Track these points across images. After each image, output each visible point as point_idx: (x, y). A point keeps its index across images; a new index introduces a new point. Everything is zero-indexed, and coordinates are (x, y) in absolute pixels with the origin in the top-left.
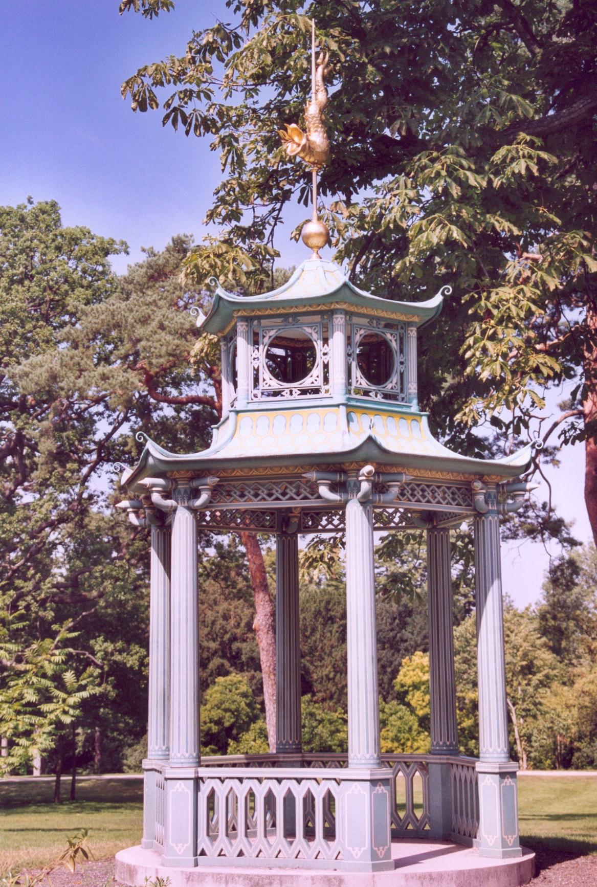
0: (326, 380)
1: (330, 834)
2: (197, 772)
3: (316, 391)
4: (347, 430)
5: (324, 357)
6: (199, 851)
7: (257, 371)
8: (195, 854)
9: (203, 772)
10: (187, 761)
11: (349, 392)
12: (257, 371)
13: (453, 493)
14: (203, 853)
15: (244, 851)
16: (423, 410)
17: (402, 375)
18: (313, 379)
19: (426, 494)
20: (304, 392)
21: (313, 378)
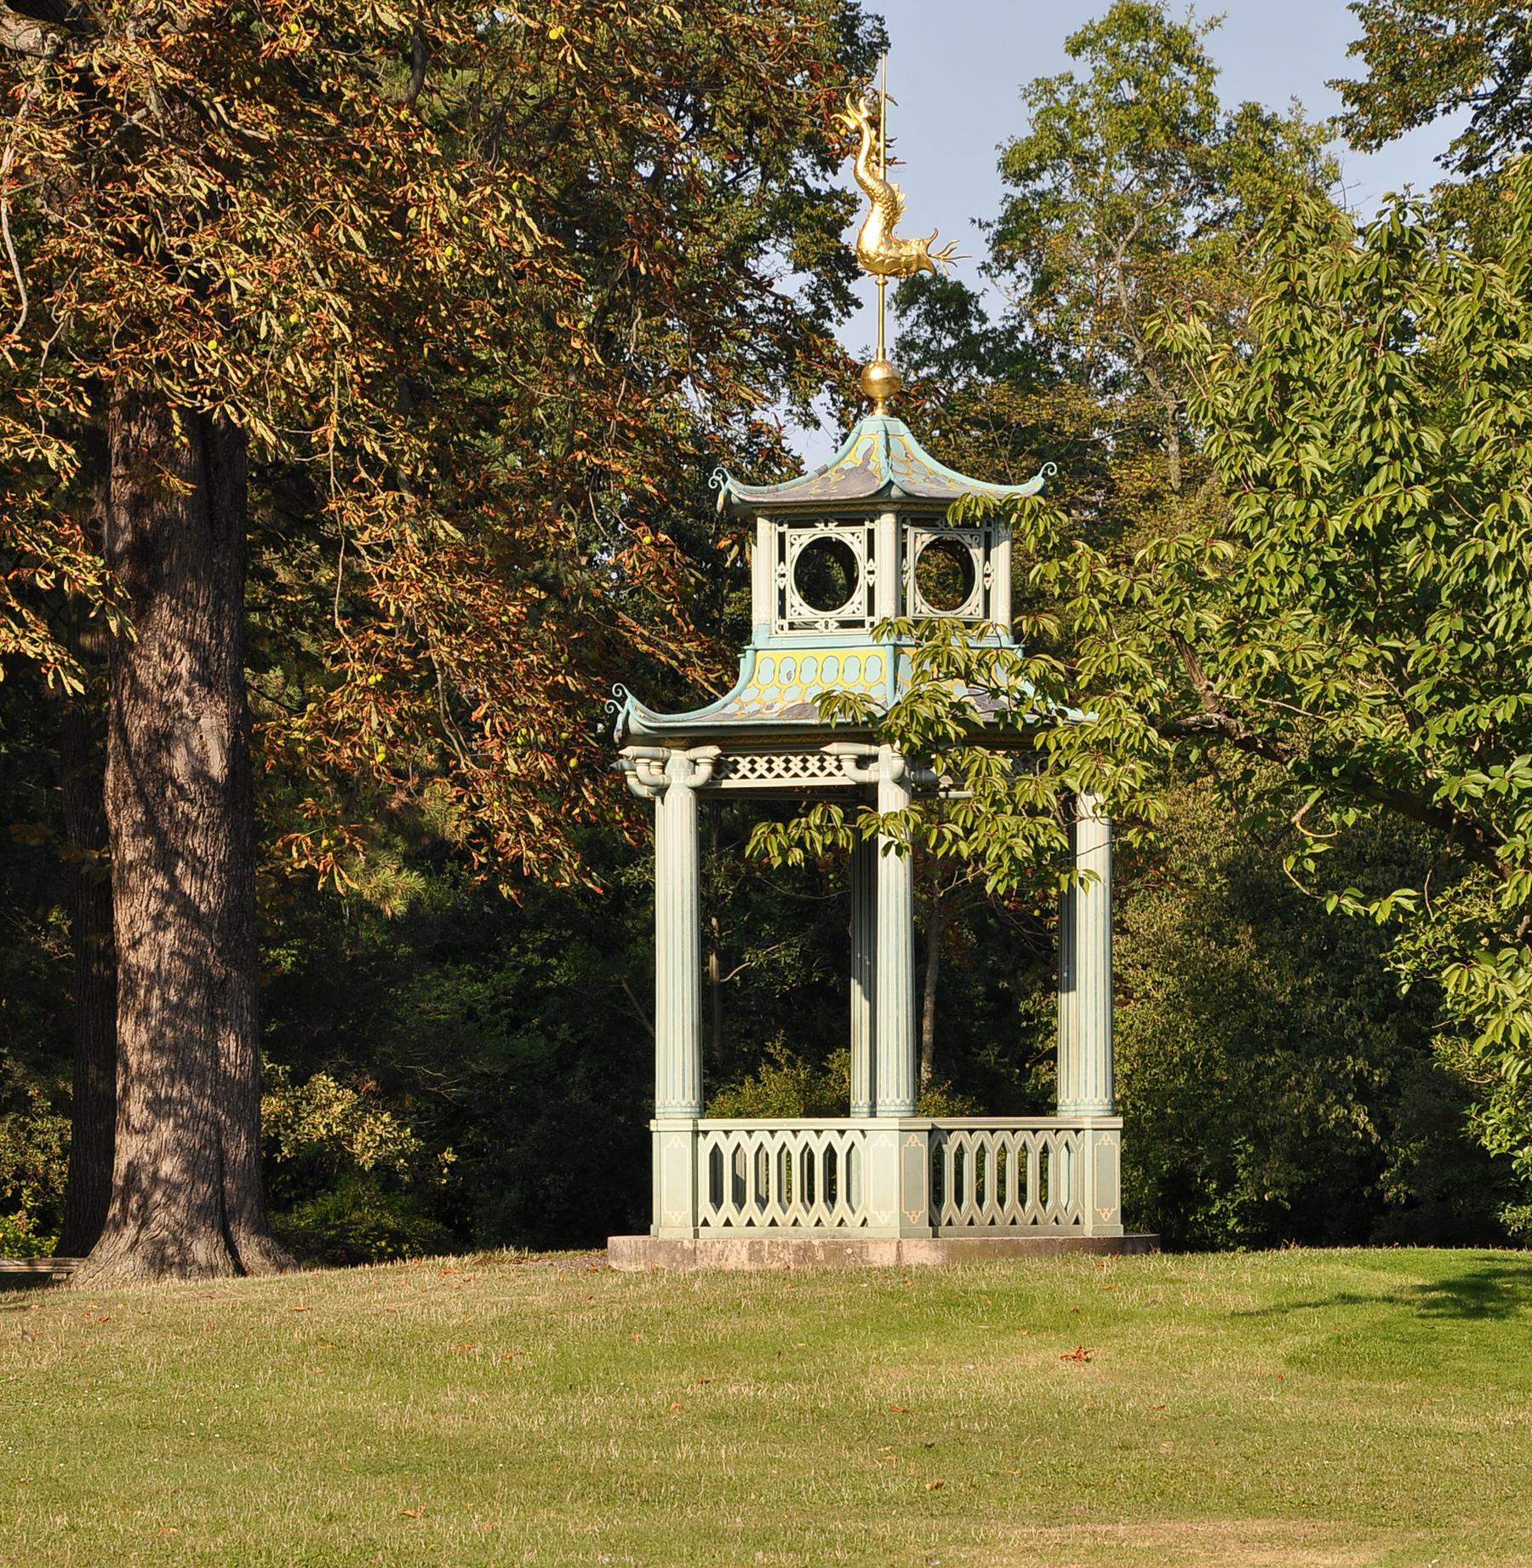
8: (695, 1224)
9: (704, 1124)
14: (706, 1223)
17: (987, 593)
18: (853, 608)
20: (845, 624)
21: (854, 607)
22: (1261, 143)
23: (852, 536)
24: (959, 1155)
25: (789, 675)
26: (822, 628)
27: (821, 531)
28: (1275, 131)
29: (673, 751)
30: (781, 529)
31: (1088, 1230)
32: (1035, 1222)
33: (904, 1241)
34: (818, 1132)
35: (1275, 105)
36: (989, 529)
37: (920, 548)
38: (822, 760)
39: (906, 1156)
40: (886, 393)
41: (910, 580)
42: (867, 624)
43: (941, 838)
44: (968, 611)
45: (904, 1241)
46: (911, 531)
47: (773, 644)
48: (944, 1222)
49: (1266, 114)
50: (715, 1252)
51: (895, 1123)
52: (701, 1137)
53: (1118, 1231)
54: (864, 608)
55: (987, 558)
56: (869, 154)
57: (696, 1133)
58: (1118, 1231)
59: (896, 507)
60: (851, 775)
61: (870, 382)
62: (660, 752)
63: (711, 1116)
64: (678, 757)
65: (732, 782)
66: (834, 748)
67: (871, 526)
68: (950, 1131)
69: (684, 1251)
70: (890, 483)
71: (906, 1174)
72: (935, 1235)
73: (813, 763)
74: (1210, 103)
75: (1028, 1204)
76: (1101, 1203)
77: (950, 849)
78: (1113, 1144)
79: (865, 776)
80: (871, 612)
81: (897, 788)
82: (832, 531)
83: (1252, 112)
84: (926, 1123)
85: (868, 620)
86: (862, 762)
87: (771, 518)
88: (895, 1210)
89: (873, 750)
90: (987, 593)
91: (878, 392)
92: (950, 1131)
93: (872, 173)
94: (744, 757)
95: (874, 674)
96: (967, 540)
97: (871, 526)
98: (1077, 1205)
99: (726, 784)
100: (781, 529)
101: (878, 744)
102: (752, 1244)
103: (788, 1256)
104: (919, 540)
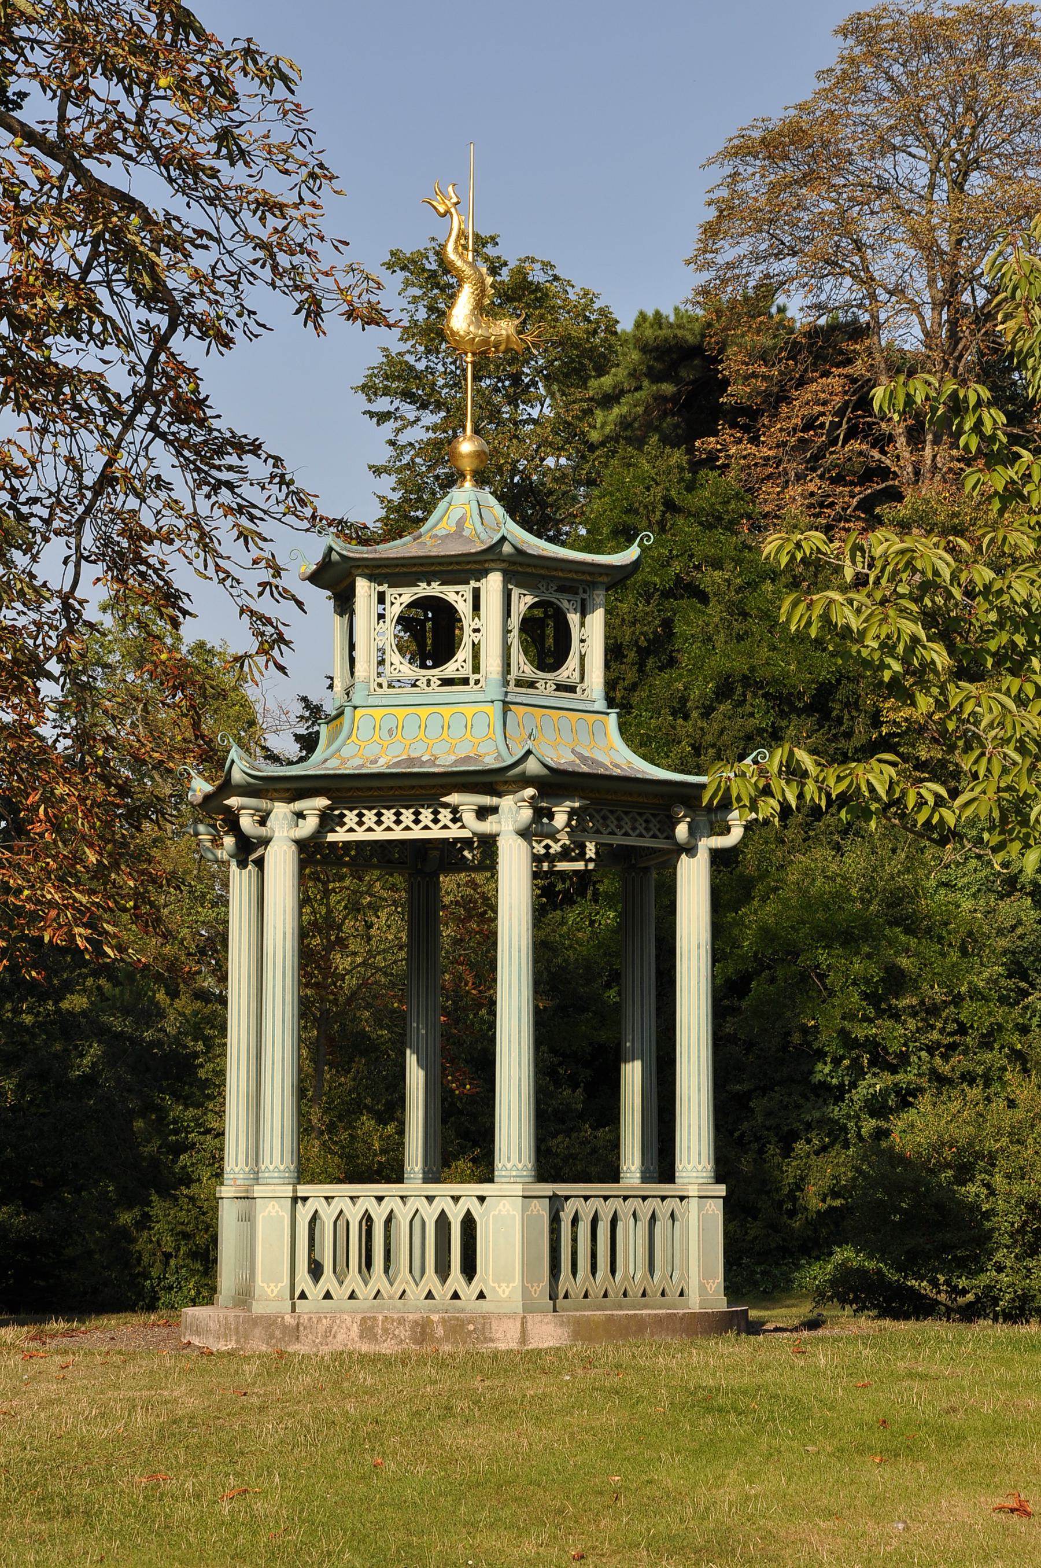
0: (476, 669)
1: (469, 1269)
2: (295, 1191)
3: (465, 681)
4: (578, 749)
5: (473, 635)
6: (297, 1294)
7: (382, 651)
8: (292, 1298)
9: (303, 1190)
10: (282, 1175)
11: (506, 683)
12: (382, 651)
13: (647, 821)
14: (303, 1296)
15: (357, 1291)
16: (610, 706)
17: (582, 658)
18: (458, 665)
19: (651, 826)
20: (447, 682)
21: (458, 665)
22: (206, 661)
23: (457, 596)
24: (575, 1221)
25: (390, 731)
26: (424, 686)
27: (424, 590)
28: (214, 655)
29: (276, 804)
30: (381, 589)
31: (694, 1304)
32: (644, 1295)
33: (529, 1316)
34: (380, 1199)
35: (213, 642)
36: (585, 596)
37: (523, 609)
38: (436, 813)
39: (528, 1223)
40: (474, 467)
41: (514, 638)
42: (472, 682)
43: (921, 803)
44: (565, 674)
45: (529, 1316)
46: (515, 592)
47: (371, 701)
48: (561, 1295)
49: (208, 646)
50: (321, 1329)
51: (518, 1189)
52: (299, 1204)
53: (720, 1303)
54: (469, 666)
55: (582, 624)
56: (458, 237)
57: (295, 1199)
58: (720, 1303)
59: (504, 565)
60: (473, 825)
61: (460, 455)
62: (263, 804)
63: (311, 1182)
64: (281, 811)
65: (339, 836)
66: (453, 799)
67: (477, 585)
68: (567, 1198)
69: (284, 1327)
70: (503, 539)
71: (528, 1243)
72: (555, 1311)
73: (426, 815)
74: (179, 639)
75: (600, 1274)
76: (706, 1274)
77: (931, 816)
78: (716, 1209)
79: (487, 827)
80: (476, 669)
81: (520, 841)
82: (435, 589)
83: (201, 645)
84: (547, 1189)
85: (473, 678)
86: (483, 813)
87: (371, 578)
88: (517, 1282)
89: (493, 801)
90: (582, 658)
91: (467, 466)
92: (567, 1198)
93: (461, 256)
94: (351, 810)
95: (481, 730)
96: (565, 605)
97: (477, 585)
98: (682, 1277)
99: (331, 837)
100: (381, 589)
101: (500, 795)
102: (364, 1320)
103: (403, 1333)
104: (523, 602)
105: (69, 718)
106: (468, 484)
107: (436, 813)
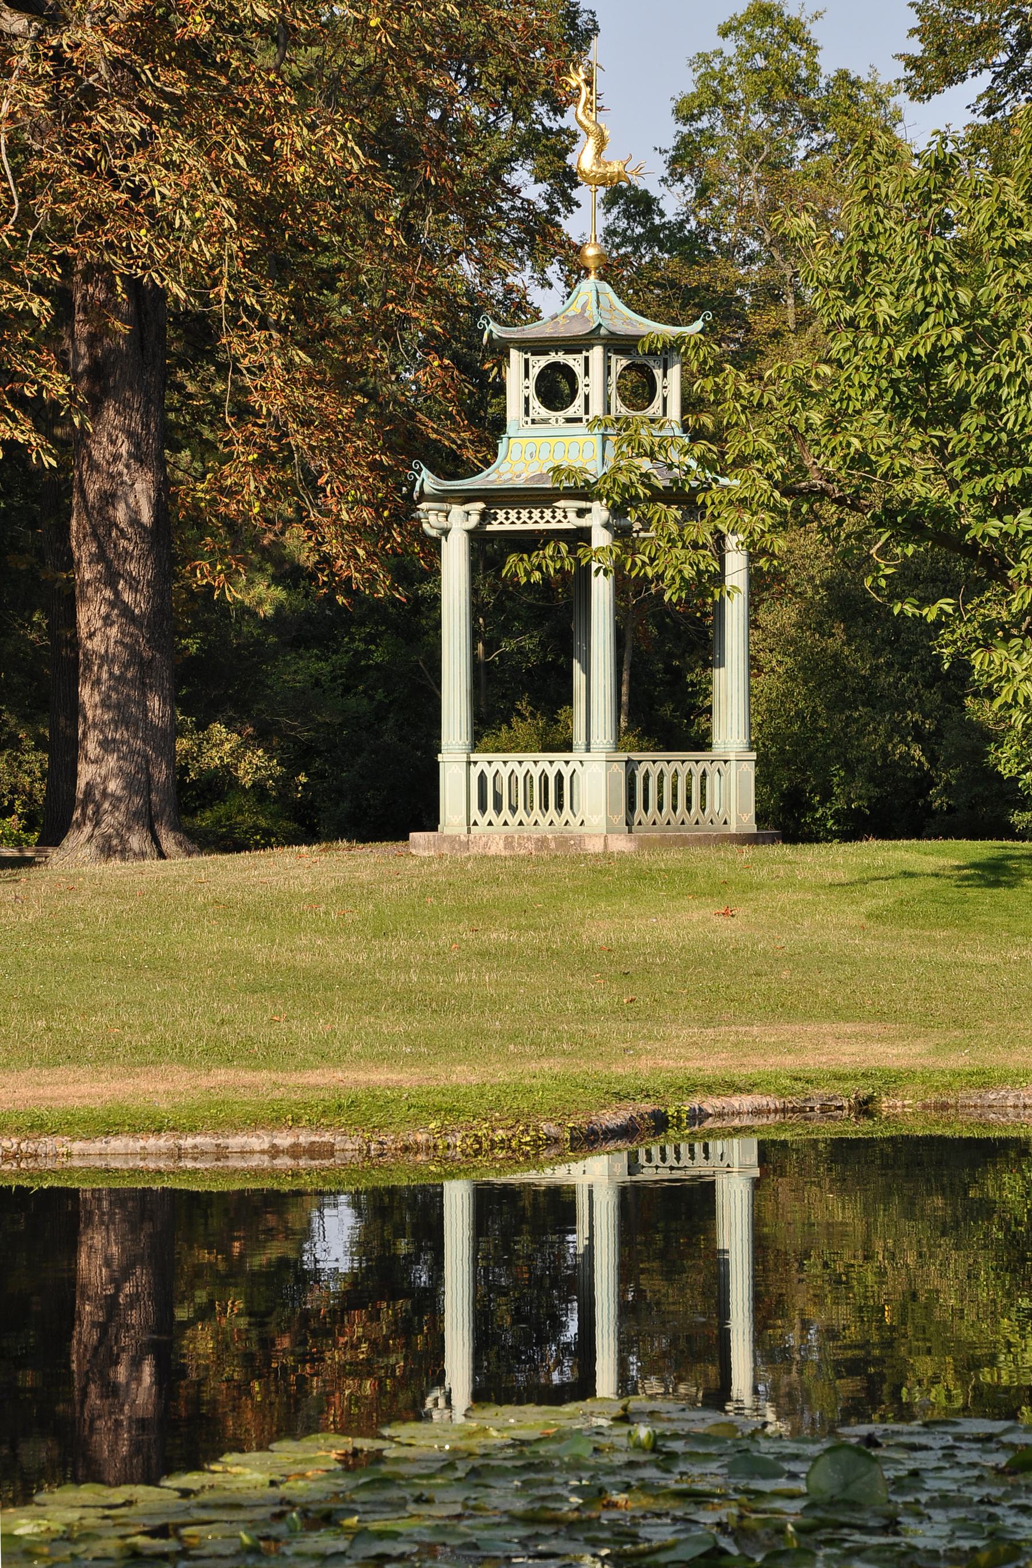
8: (468, 824)
9: (474, 757)
14: (475, 824)
17: (665, 399)
20: (569, 420)
21: (576, 409)
22: (850, 96)
27: (553, 357)
28: (859, 89)
31: (733, 828)
32: (697, 823)
35: (859, 71)
37: (619, 369)
38: (554, 512)
39: (610, 778)
41: (613, 390)
43: (634, 564)
46: (614, 357)
47: (521, 433)
49: (853, 77)
50: (482, 843)
51: (603, 756)
53: (753, 829)
54: (582, 409)
55: (665, 375)
57: (469, 763)
60: (573, 522)
62: (444, 506)
63: (479, 752)
64: (457, 510)
65: (493, 527)
66: (562, 503)
68: (640, 762)
69: (460, 843)
70: (600, 325)
71: (610, 791)
73: (548, 513)
74: (815, 69)
75: (650, 810)
76: (742, 810)
78: (750, 770)
79: (582, 522)
80: (587, 412)
81: (604, 531)
82: (561, 357)
83: (843, 76)
84: (624, 756)
86: (581, 513)
87: (519, 349)
88: (603, 815)
89: (588, 505)
90: (665, 399)
91: (591, 264)
92: (640, 762)
93: (587, 117)
95: (588, 454)
96: (651, 363)
98: (725, 812)
99: (489, 528)
103: (531, 846)
104: (619, 363)
105: (682, 175)
106: (592, 277)
107: (554, 512)
